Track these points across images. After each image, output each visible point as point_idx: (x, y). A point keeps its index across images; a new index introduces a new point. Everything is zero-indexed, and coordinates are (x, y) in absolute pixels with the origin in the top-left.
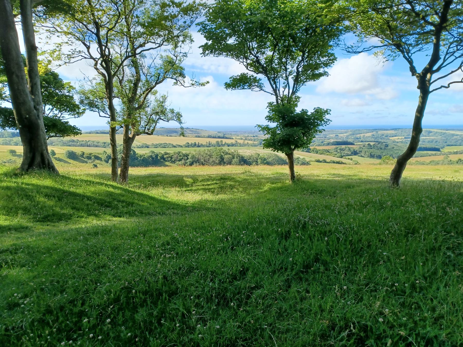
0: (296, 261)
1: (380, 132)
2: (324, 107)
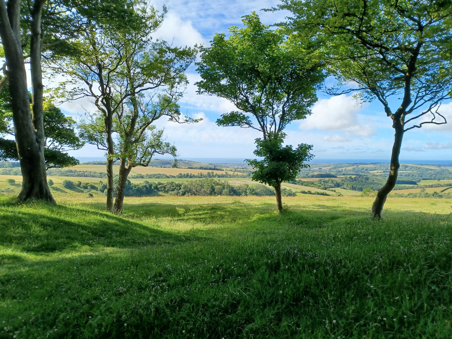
0: (286, 293)
1: (360, 166)
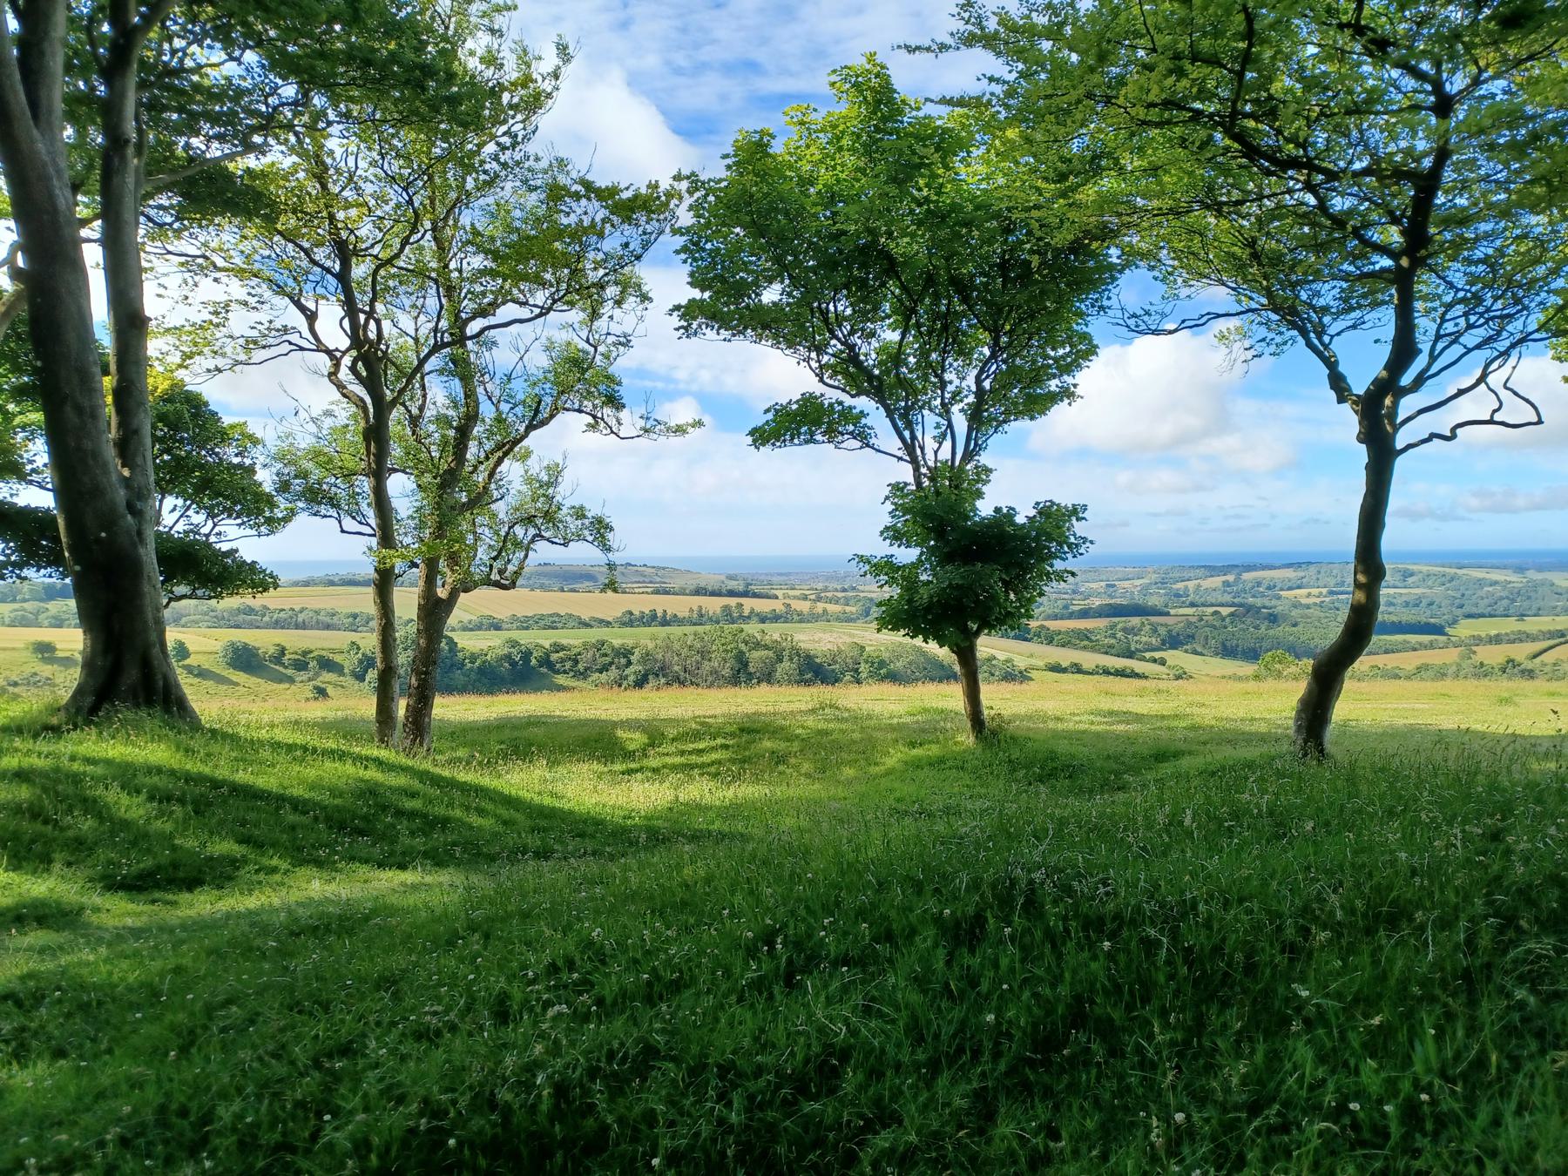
0: (1010, 1022)
2: (1065, 499)
